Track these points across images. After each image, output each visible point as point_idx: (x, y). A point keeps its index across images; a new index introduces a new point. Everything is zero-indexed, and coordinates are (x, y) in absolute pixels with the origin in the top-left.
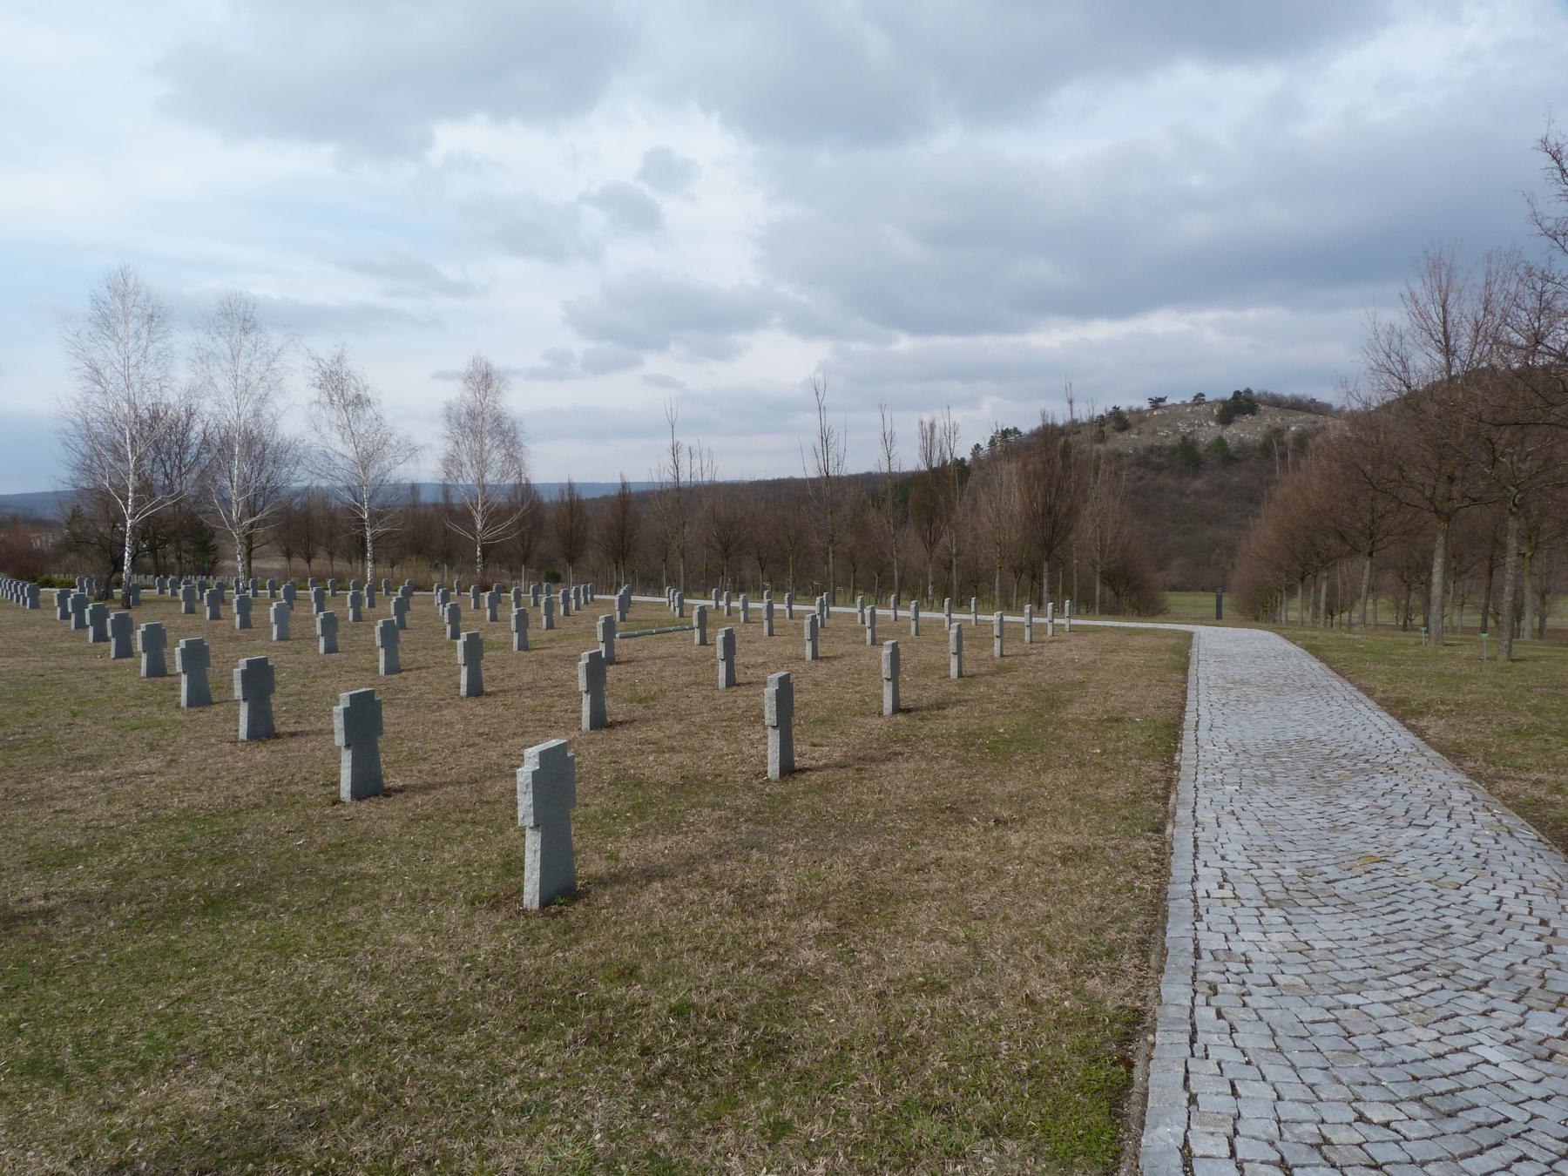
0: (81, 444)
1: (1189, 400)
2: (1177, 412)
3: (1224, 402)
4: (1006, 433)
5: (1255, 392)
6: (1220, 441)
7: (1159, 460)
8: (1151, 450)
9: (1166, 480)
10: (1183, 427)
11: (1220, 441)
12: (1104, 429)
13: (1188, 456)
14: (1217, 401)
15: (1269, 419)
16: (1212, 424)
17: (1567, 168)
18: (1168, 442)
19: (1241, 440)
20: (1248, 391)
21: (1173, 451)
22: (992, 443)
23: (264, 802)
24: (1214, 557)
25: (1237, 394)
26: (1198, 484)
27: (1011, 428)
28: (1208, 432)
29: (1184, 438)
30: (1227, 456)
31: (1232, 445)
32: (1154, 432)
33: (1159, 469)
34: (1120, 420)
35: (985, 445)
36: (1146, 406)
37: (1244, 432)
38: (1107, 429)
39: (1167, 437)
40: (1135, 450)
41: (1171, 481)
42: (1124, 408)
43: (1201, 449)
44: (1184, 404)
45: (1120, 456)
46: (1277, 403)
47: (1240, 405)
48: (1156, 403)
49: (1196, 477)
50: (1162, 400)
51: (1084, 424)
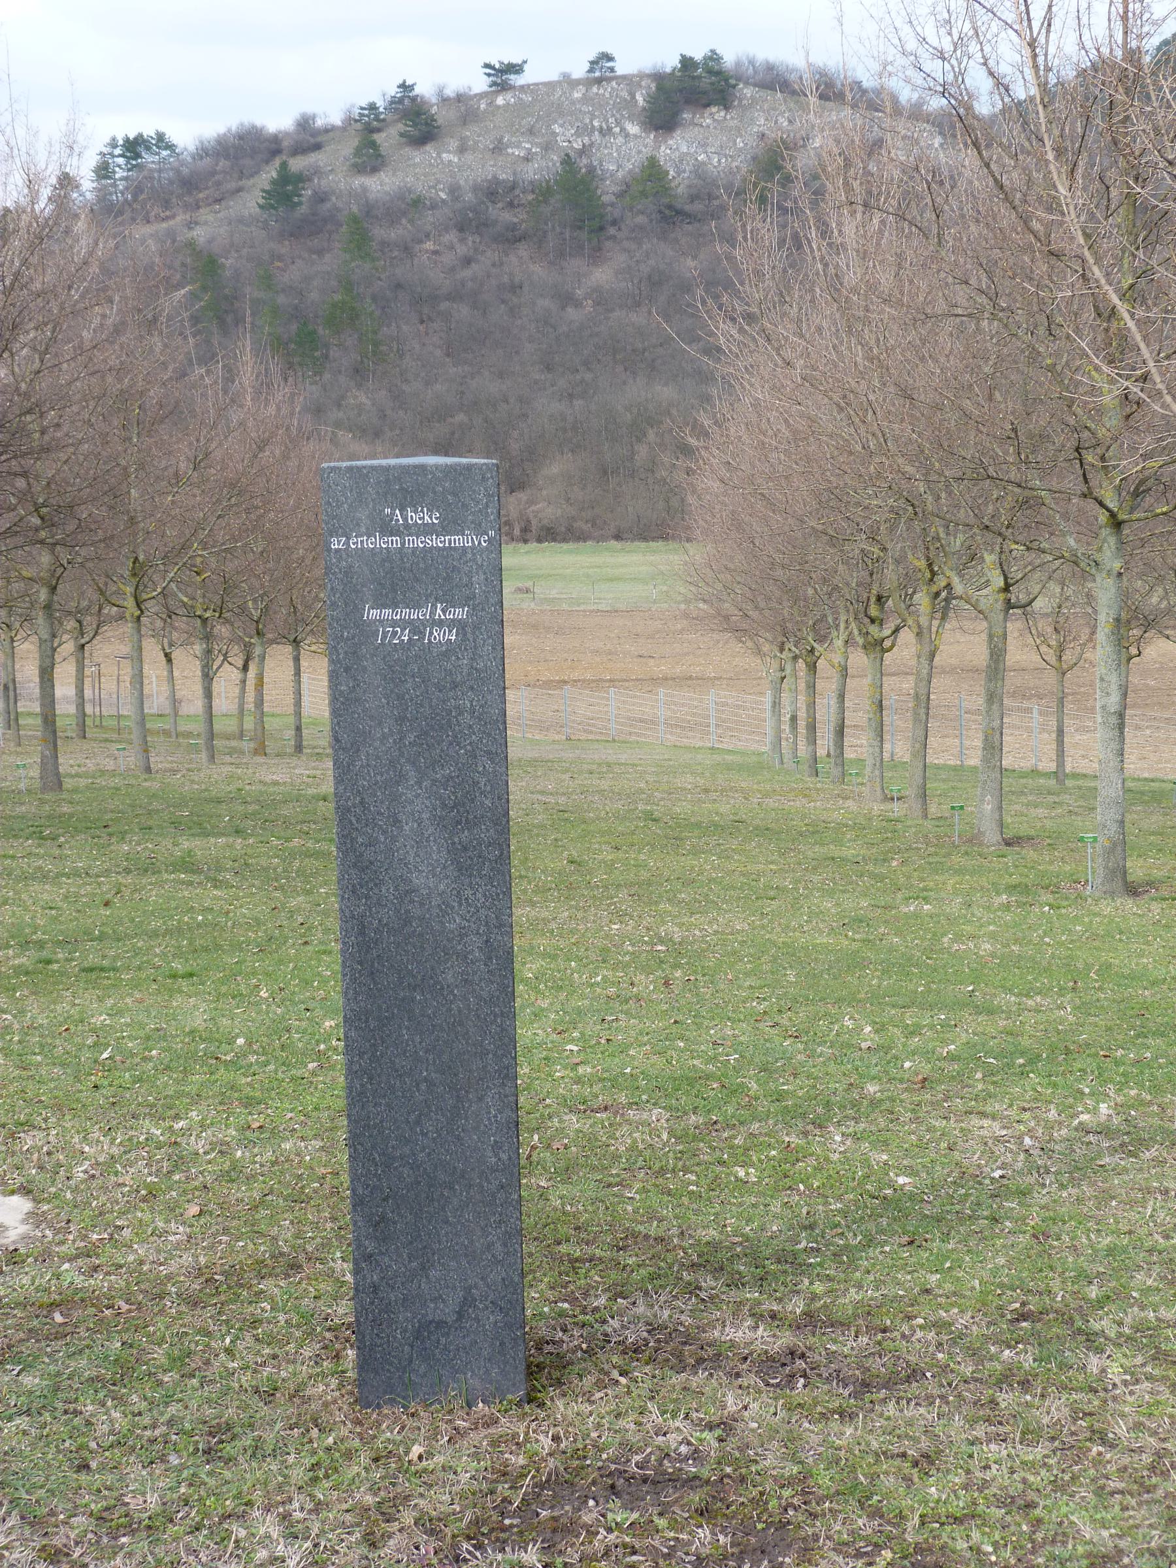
0: (724, 332)
1: (579, 70)
2: (551, 99)
3: (659, 78)
4: (134, 147)
5: (729, 58)
6: (653, 171)
7: (507, 217)
8: (492, 191)
9: (524, 265)
10: (566, 136)
11: (653, 171)
12: (378, 138)
13: (574, 209)
14: (642, 76)
15: (765, 120)
16: (633, 129)
17: (1119, 87)
18: (532, 172)
19: (699, 170)
20: (714, 57)
21: (543, 192)
22: (103, 171)
23: (1106, 314)
24: (642, 451)
25: (687, 63)
26: (602, 276)
27: (149, 132)
28: (624, 150)
29: (567, 161)
30: (671, 208)
31: (680, 181)
32: (498, 148)
33: (511, 238)
34: (415, 118)
35: (84, 171)
36: (480, 83)
37: (703, 148)
38: (387, 139)
39: (531, 161)
40: (454, 190)
41: (538, 270)
42: (424, 89)
43: (608, 191)
44: (568, 82)
45: (416, 204)
46: (775, 81)
47: (695, 88)
48: (503, 75)
49: (596, 255)
50: (515, 69)
51: (328, 130)
